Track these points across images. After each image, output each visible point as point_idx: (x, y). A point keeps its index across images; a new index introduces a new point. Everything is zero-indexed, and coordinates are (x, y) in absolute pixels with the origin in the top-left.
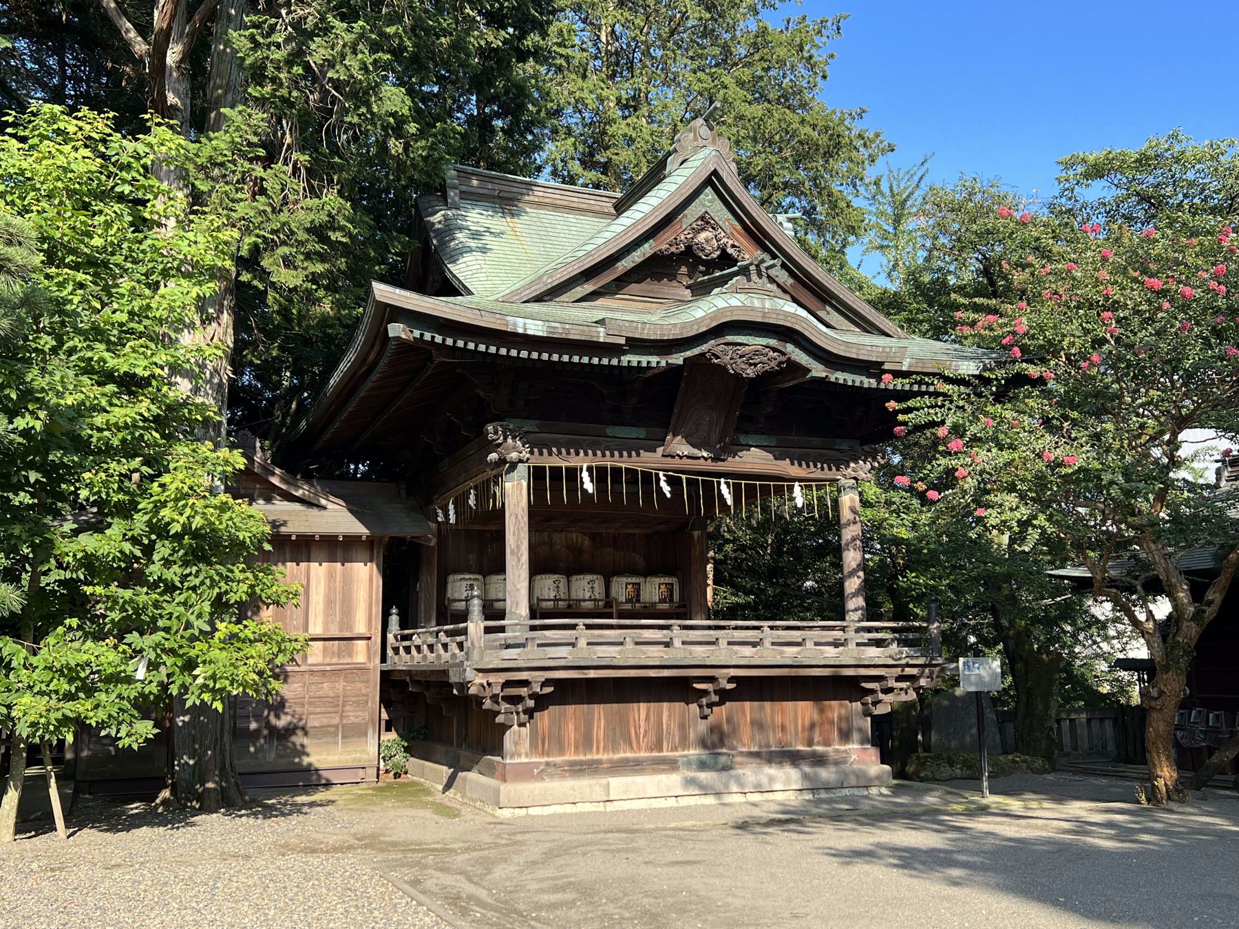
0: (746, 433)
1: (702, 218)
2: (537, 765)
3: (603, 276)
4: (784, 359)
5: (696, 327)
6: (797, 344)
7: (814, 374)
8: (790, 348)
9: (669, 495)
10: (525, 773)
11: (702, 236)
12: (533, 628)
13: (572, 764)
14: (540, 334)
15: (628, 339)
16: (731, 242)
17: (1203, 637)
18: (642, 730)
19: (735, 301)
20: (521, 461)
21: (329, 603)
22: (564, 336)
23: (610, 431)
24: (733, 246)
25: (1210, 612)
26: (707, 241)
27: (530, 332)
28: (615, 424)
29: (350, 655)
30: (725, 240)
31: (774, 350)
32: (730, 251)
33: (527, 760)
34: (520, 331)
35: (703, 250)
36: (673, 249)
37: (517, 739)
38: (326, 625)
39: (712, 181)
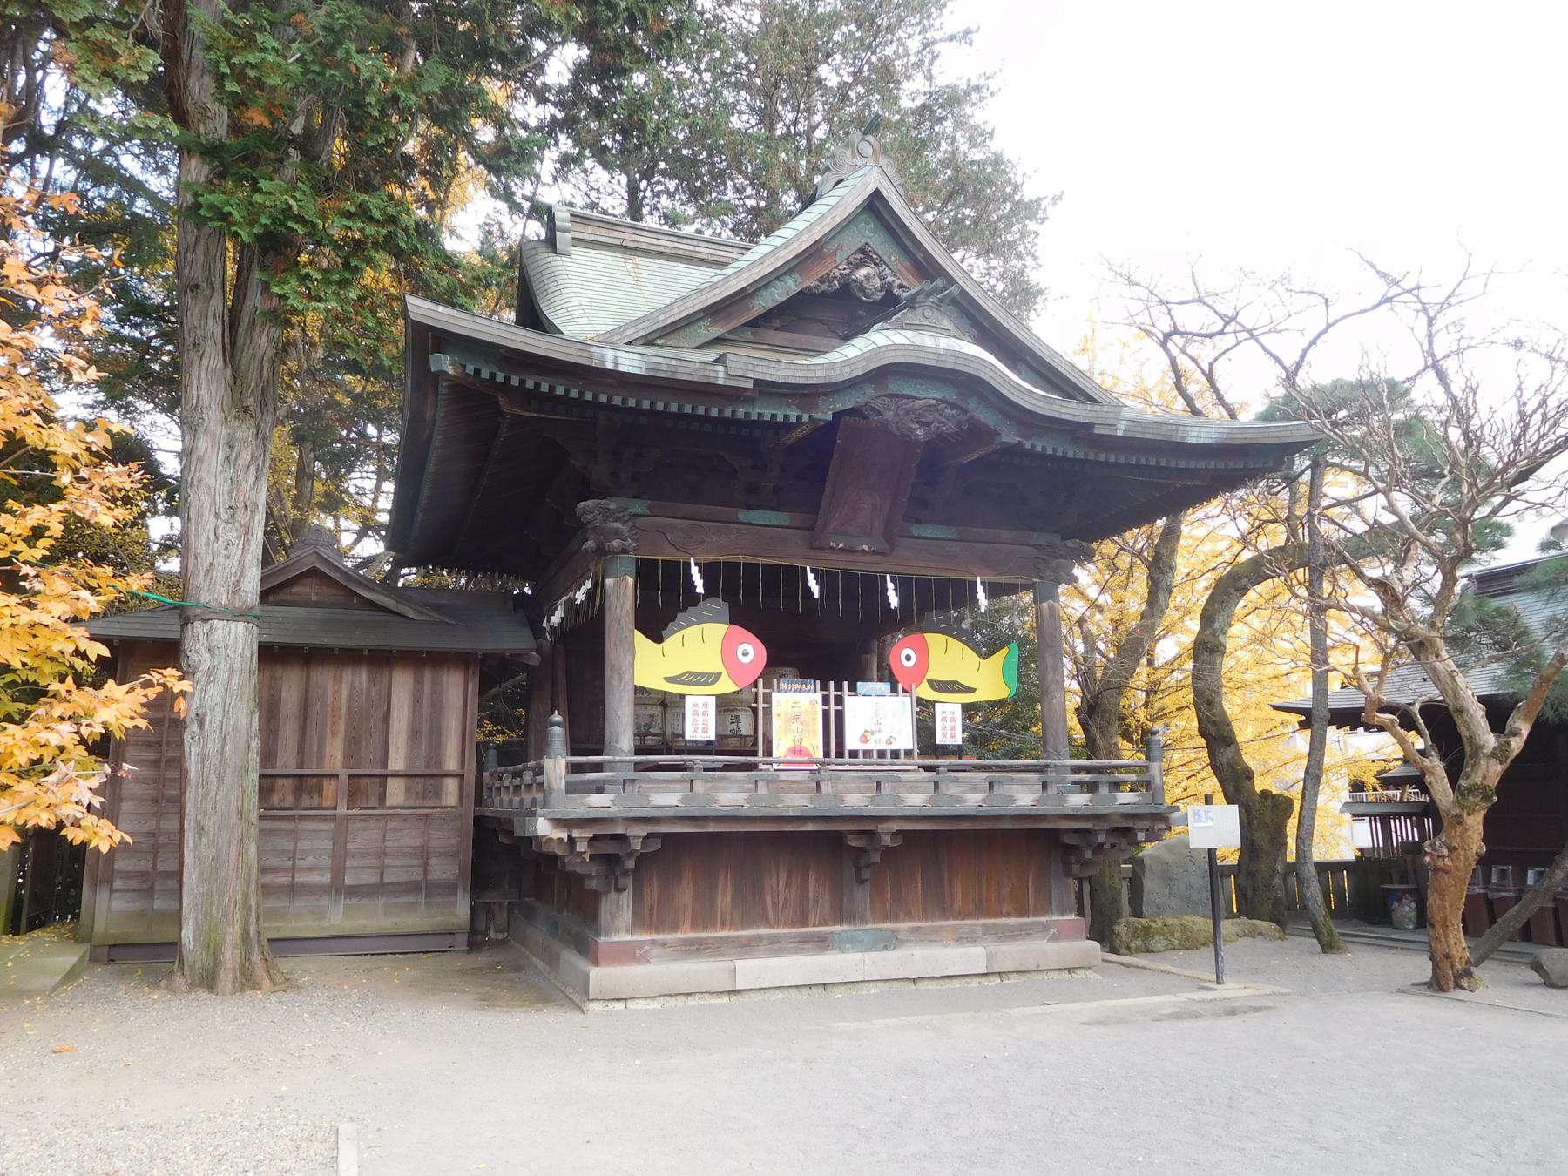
0: (919, 521)
1: (862, 250)
2: (641, 944)
3: (737, 317)
4: (965, 418)
5: (847, 369)
6: (982, 398)
7: (1005, 439)
8: (972, 404)
9: (816, 595)
10: (627, 954)
11: (862, 272)
12: (639, 767)
13: (687, 943)
14: (637, 371)
15: (757, 382)
16: (897, 282)
17: (1505, 778)
18: (781, 899)
19: (900, 338)
20: (625, 551)
21: (414, 733)
22: (668, 375)
23: (745, 515)
24: (901, 286)
25: (1517, 744)
26: (867, 277)
27: (622, 369)
28: (750, 507)
29: (438, 796)
30: (890, 278)
31: (953, 406)
32: (896, 291)
33: (628, 938)
34: (610, 366)
35: (863, 290)
36: (824, 287)
37: (618, 911)
38: (410, 760)
39: (875, 206)
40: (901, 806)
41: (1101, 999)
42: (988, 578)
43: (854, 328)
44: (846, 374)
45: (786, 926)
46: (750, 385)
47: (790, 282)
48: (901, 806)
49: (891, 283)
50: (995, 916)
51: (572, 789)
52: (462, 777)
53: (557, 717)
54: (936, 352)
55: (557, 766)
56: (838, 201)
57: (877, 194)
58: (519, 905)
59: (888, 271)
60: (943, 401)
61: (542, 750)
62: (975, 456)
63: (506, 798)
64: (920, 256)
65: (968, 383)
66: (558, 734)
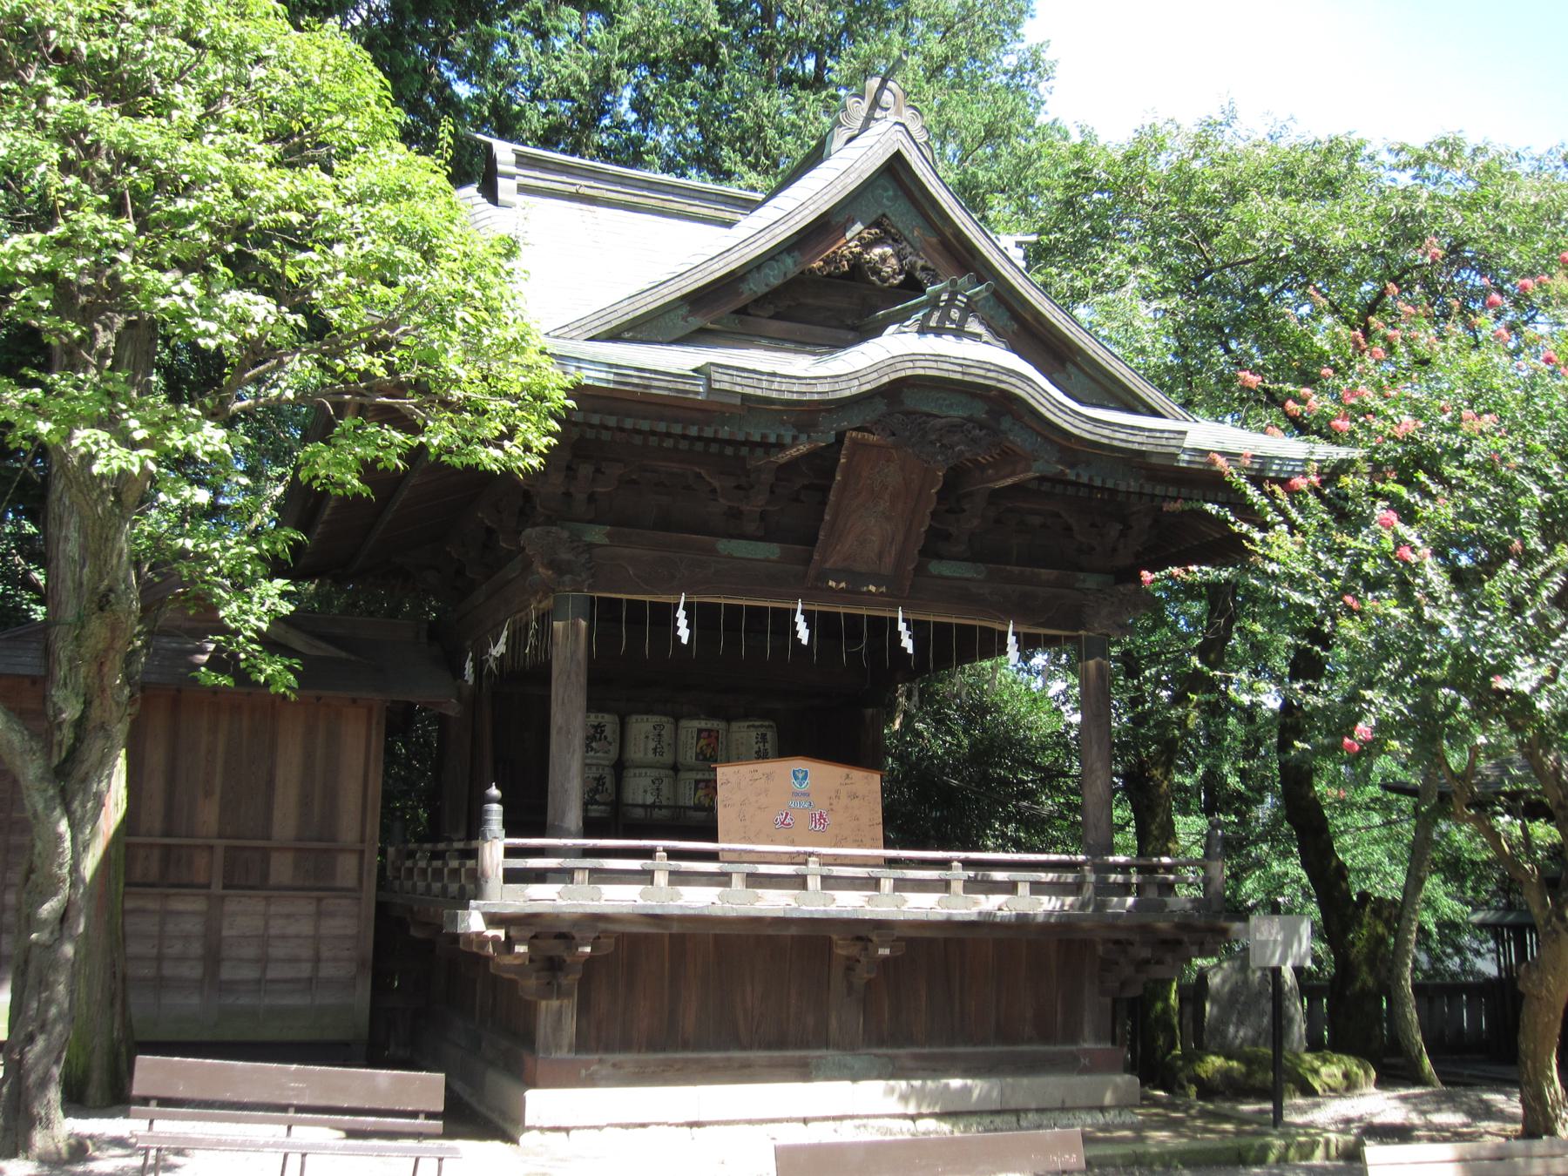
11: (877, 252)
16: (920, 263)
26: (883, 259)
28: (731, 536)
35: (877, 272)
39: (896, 167)
40: (904, 908)
41: (727, 1049)
42: (1023, 629)
43: (866, 330)
44: (854, 389)
45: (966, 1044)
46: (738, 401)
47: (789, 261)
48: (904, 908)
49: (913, 266)
50: (1015, 1043)
51: (511, 876)
52: (362, 853)
53: (494, 791)
54: (964, 365)
55: (494, 852)
56: (849, 164)
57: (898, 156)
58: (452, 1023)
59: (909, 250)
60: (970, 419)
61: (475, 828)
62: (1009, 481)
63: (421, 885)
64: (948, 232)
65: (1000, 404)
66: (495, 812)
